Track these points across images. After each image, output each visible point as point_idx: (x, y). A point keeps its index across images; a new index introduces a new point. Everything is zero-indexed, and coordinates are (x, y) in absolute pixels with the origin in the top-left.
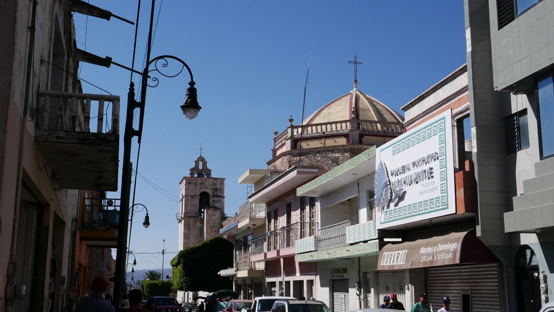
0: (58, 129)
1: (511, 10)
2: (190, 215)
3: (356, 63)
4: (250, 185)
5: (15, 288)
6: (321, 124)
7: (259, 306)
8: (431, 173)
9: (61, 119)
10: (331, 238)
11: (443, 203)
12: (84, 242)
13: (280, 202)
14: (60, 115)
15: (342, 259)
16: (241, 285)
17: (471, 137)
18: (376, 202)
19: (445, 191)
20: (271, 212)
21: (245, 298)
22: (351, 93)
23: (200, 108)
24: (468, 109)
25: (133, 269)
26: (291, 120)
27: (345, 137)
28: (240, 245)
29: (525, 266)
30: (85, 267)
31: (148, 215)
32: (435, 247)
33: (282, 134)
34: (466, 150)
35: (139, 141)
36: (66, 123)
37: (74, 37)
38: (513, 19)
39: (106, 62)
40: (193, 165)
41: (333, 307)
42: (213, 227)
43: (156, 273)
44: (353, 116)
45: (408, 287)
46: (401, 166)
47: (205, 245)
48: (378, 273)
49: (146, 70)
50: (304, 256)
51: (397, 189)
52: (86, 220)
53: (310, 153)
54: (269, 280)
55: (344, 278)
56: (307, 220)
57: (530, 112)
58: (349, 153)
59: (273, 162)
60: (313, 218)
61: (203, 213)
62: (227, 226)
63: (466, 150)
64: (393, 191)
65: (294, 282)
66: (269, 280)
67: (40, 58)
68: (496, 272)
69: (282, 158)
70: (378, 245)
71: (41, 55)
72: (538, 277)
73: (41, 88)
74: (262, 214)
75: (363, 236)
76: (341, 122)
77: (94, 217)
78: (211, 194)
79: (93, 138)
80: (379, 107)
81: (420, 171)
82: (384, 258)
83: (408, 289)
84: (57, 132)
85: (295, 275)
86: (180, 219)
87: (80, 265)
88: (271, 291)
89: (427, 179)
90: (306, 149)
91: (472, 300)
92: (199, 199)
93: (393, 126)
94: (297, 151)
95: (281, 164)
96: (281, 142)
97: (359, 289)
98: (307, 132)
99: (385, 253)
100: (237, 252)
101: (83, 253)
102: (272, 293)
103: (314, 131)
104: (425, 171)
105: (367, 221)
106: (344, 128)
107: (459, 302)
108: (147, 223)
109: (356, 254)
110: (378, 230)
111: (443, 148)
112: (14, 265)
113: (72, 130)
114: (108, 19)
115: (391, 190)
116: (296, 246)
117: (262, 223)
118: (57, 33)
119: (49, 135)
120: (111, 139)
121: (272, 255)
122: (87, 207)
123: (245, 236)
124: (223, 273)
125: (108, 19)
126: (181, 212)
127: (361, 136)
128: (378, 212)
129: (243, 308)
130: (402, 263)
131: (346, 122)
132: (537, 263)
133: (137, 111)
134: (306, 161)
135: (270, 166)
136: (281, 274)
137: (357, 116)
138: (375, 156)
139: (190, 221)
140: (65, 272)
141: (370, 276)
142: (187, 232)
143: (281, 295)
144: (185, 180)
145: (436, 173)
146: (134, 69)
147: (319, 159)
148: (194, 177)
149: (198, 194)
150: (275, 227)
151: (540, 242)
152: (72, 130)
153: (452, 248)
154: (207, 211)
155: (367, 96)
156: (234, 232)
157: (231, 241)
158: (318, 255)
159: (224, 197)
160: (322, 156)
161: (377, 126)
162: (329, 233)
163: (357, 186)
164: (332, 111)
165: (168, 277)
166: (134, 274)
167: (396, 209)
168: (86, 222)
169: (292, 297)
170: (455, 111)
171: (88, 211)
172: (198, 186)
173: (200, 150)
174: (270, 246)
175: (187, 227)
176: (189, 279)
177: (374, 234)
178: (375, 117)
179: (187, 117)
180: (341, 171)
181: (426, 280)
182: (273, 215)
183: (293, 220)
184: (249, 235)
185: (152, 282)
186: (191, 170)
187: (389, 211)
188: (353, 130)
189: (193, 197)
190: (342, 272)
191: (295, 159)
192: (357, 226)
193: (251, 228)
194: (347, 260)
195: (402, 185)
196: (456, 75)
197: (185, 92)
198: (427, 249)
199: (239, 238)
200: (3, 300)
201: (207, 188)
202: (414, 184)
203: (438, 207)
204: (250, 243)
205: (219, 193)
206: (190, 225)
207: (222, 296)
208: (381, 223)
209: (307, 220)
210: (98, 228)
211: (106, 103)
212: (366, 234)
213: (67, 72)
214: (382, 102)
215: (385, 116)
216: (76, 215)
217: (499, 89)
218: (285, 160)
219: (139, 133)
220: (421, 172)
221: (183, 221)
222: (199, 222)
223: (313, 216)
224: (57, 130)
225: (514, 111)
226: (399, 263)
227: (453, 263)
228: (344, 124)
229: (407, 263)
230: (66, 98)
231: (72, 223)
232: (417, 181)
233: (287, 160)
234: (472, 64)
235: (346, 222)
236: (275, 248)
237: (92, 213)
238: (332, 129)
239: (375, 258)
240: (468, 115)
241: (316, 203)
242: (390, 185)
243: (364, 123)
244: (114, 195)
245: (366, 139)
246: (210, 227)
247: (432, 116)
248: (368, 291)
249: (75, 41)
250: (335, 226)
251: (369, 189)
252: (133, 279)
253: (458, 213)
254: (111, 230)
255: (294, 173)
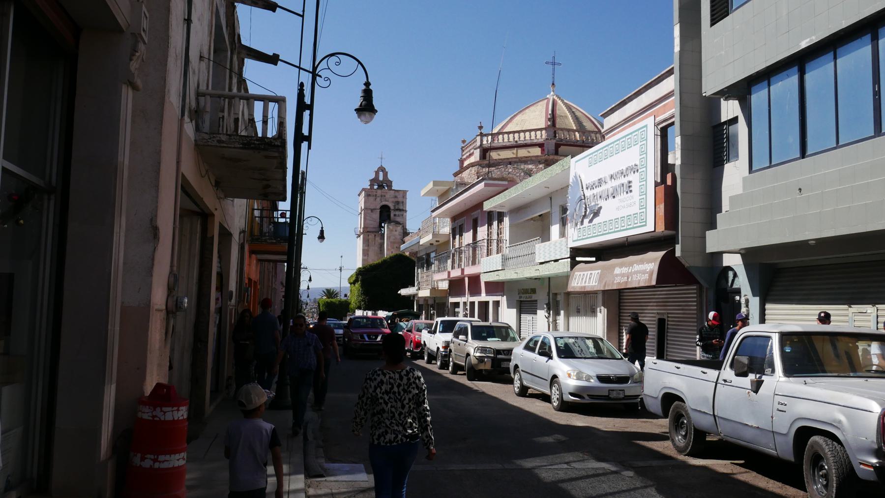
0: (220, 132)
1: (726, 4)
2: (369, 230)
3: (554, 65)
4: (434, 198)
5: (177, 300)
6: (514, 132)
7: (441, 327)
8: (630, 187)
9: (223, 121)
10: (519, 256)
11: (642, 220)
12: (254, 256)
13: (465, 217)
14: (221, 116)
15: (531, 279)
16: (422, 305)
17: (675, 148)
18: (569, 218)
19: (643, 207)
20: (456, 227)
21: (426, 318)
22: (548, 98)
23: (377, 111)
24: (673, 117)
25: (308, 286)
26: (481, 128)
27: (539, 147)
28: (422, 263)
29: (726, 288)
30: (255, 282)
31: (371, 87)
32: (631, 267)
33: (470, 142)
34: (669, 162)
35: (309, 147)
36: (230, 127)
37: (238, 31)
38: (728, 15)
39: (273, 59)
40: (373, 176)
41: (520, 330)
42: (394, 243)
43: (333, 291)
44: (549, 123)
45: (601, 309)
46: (597, 179)
47: (385, 261)
48: (568, 294)
49: (315, 68)
50: (491, 275)
51: (592, 204)
52: (256, 232)
53: (501, 164)
54: (452, 300)
55: (533, 299)
56: (495, 236)
57: (742, 121)
58: (543, 165)
59: (460, 174)
60: (501, 234)
61: (384, 227)
62: (409, 241)
63: (669, 162)
64: (587, 206)
65: (480, 303)
66: (452, 300)
67: (199, 54)
68: (695, 295)
69: (470, 169)
70: (569, 265)
71: (200, 51)
72: (739, 301)
73: (201, 88)
74: (446, 230)
75: (553, 255)
76: (536, 130)
77: (264, 230)
78: (392, 208)
79: (258, 143)
80: (577, 114)
81: (617, 185)
82: (575, 279)
83: (601, 312)
84: (219, 136)
85: (481, 296)
86: (359, 233)
87: (250, 280)
88: (455, 312)
89: (625, 193)
90: (496, 160)
91: (668, 324)
92: (379, 212)
93: (593, 135)
94: (486, 162)
95: (468, 176)
96: (469, 151)
97: (549, 309)
98: (498, 140)
99: (576, 273)
100: (419, 270)
101: (254, 267)
102: (455, 314)
103: (506, 140)
104: (623, 185)
105: (560, 238)
106: (539, 136)
107: (655, 326)
108: (321, 237)
109: (546, 273)
110: (570, 248)
111: (643, 159)
112: (175, 276)
113: (235, 133)
114: (274, 11)
115: (586, 206)
116: (481, 265)
117: (445, 239)
118: (219, 27)
119: (210, 139)
120: (276, 143)
121: (456, 273)
122: (257, 218)
123: (428, 252)
124: (404, 292)
125: (274, 11)
126: (359, 226)
127: (558, 146)
128: (571, 228)
129: (424, 329)
130: (594, 284)
131: (541, 130)
132: (739, 285)
133: (306, 114)
134: (496, 172)
135: (456, 178)
136: (465, 295)
137: (554, 124)
138: (569, 167)
139: (370, 236)
140: (233, 286)
141: (560, 298)
142: (366, 248)
143: (465, 316)
144: (364, 192)
145: (635, 187)
146: (298, 69)
147: (510, 170)
148: (374, 189)
149: (378, 207)
150: (460, 243)
151: (744, 264)
152: (235, 133)
153: (649, 268)
154: (388, 226)
155: (565, 101)
156: (416, 249)
157: (413, 259)
158: (505, 275)
159: (406, 211)
160: (514, 167)
161: (575, 135)
162: (517, 251)
163: (549, 200)
164: (526, 118)
165: (346, 296)
166: (309, 291)
167: (590, 226)
168: (256, 234)
169: (476, 318)
170: (659, 119)
171: (258, 223)
172: (378, 199)
173: (380, 159)
174: (454, 264)
175: (366, 242)
176: (367, 298)
177: (566, 253)
178: (574, 125)
179: (362, 121)
180: (533, 183)
181: (620, 303)
182: (458, 230)
183: (479, 237)
184: (432, 252)
185: (329, 300)
186: (371, 181)
187: (583, 228)
188: (548, 139)
189: (372, 210)
190: (531, 293)
191: (484, 170)
192: (547, 243)
193: (434, 244)
194: (536, 280)
195: (597, 199)
196: (661, 78)
197: (319, 232)
198: (621, 269)
199: (421, 255)
200: (164, 312)
201: (388, 201)
202: (611, 198)
203: (635, 224)
204: (432, 260)
205: (400, 207)
206: (370, 241)
207: (401, 316)
208: (574, 241)
209: (495, 236)
210: (268, 241)
211: (271, 105)
212: (557, 252)
213: (231, 70)
214: (581, 108)
215: (584, 124)
216: (244, 226)
217: (708, 94)
218: (473, 171)
219: (308, 139)
220: (619, 186)
221: (362, 236)
222: (379, 238)
223: (501, 232)
224: (219, 134)
225: (723, 119)
226: (591, 284)
227: (649, 285)
228: (539, 133)
229: (599, 285)
230: (231, 98)
231: (239, 236)
232: (613, 195)
233: (475, 171)
234: (680, 66)
235: (536, 240)
236: (459, 266)
237: (261, 225)
238: (525, 137)
239: (566, 278)
240: (673, 124)
241: (505, 218)
242: (585, 199)
243: (561, 132)
244: (284, 206)
245: (562, 149)
246: (391, 244)
247: (634, 124)
248: (557, 313)
249: (239, 36)
250: (524, 243)
251: (562, 203)
252: (308, 297)
253: (656, 231)
254: (282, 244)
255: (482, 185)
